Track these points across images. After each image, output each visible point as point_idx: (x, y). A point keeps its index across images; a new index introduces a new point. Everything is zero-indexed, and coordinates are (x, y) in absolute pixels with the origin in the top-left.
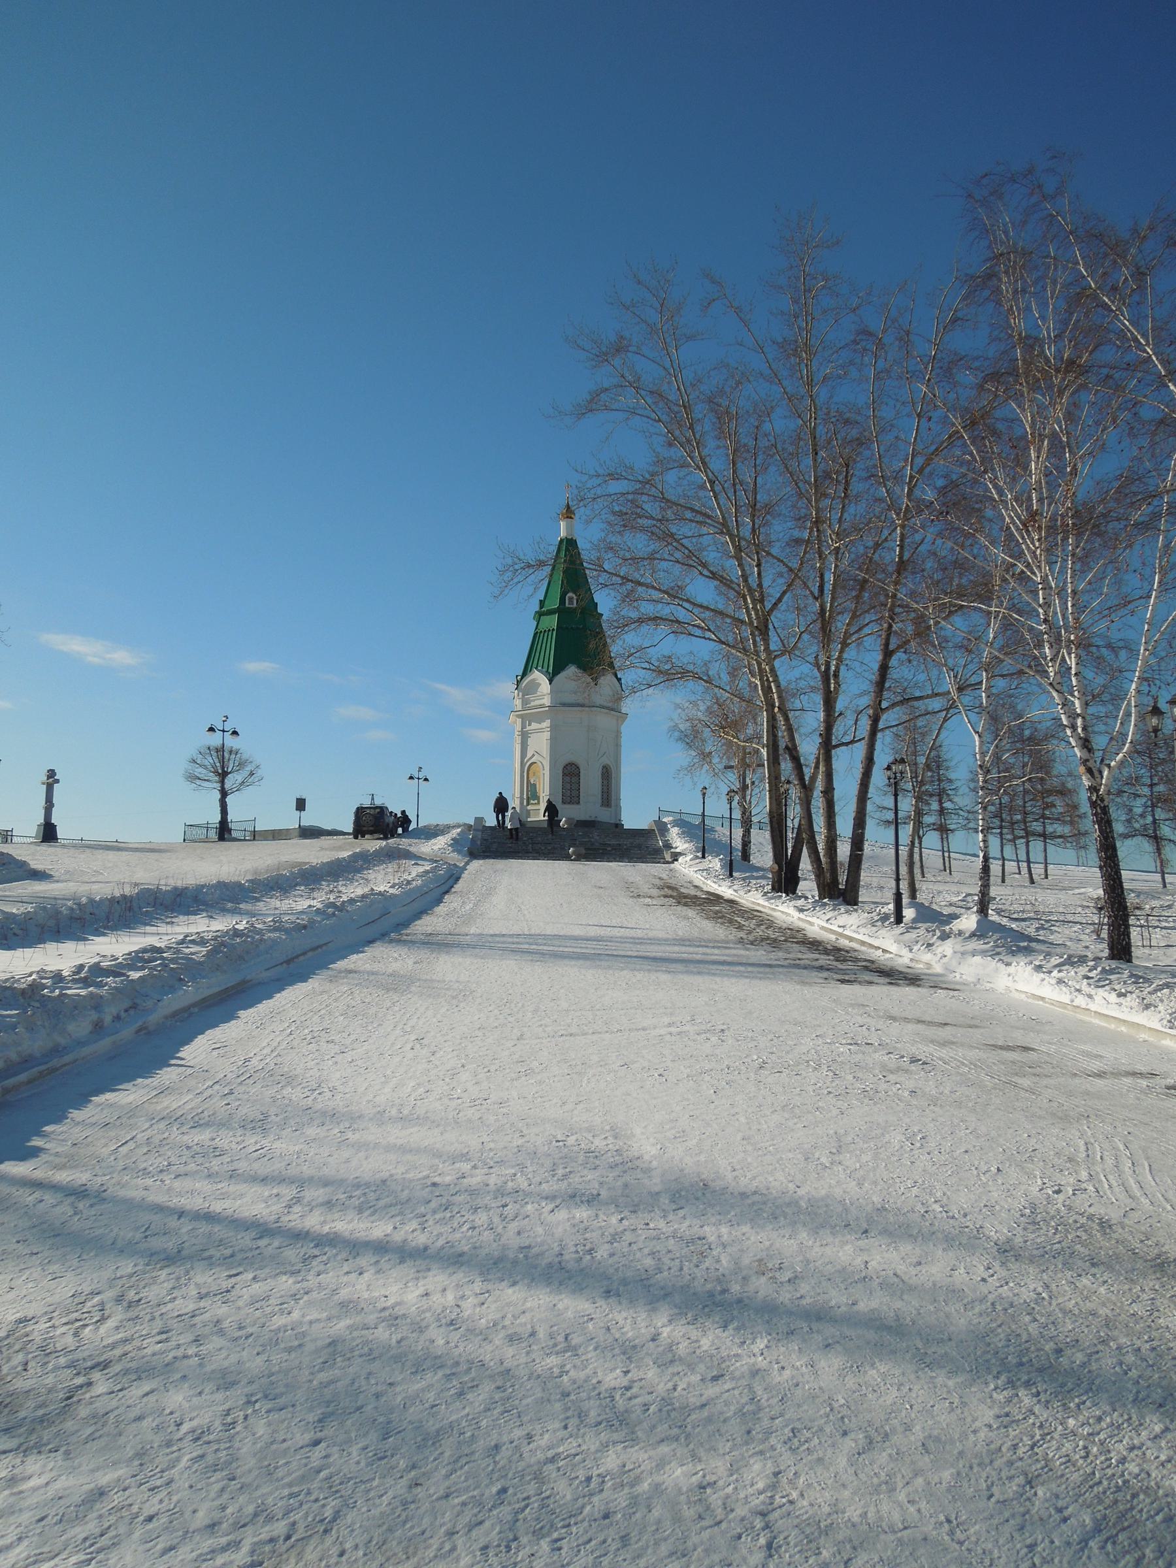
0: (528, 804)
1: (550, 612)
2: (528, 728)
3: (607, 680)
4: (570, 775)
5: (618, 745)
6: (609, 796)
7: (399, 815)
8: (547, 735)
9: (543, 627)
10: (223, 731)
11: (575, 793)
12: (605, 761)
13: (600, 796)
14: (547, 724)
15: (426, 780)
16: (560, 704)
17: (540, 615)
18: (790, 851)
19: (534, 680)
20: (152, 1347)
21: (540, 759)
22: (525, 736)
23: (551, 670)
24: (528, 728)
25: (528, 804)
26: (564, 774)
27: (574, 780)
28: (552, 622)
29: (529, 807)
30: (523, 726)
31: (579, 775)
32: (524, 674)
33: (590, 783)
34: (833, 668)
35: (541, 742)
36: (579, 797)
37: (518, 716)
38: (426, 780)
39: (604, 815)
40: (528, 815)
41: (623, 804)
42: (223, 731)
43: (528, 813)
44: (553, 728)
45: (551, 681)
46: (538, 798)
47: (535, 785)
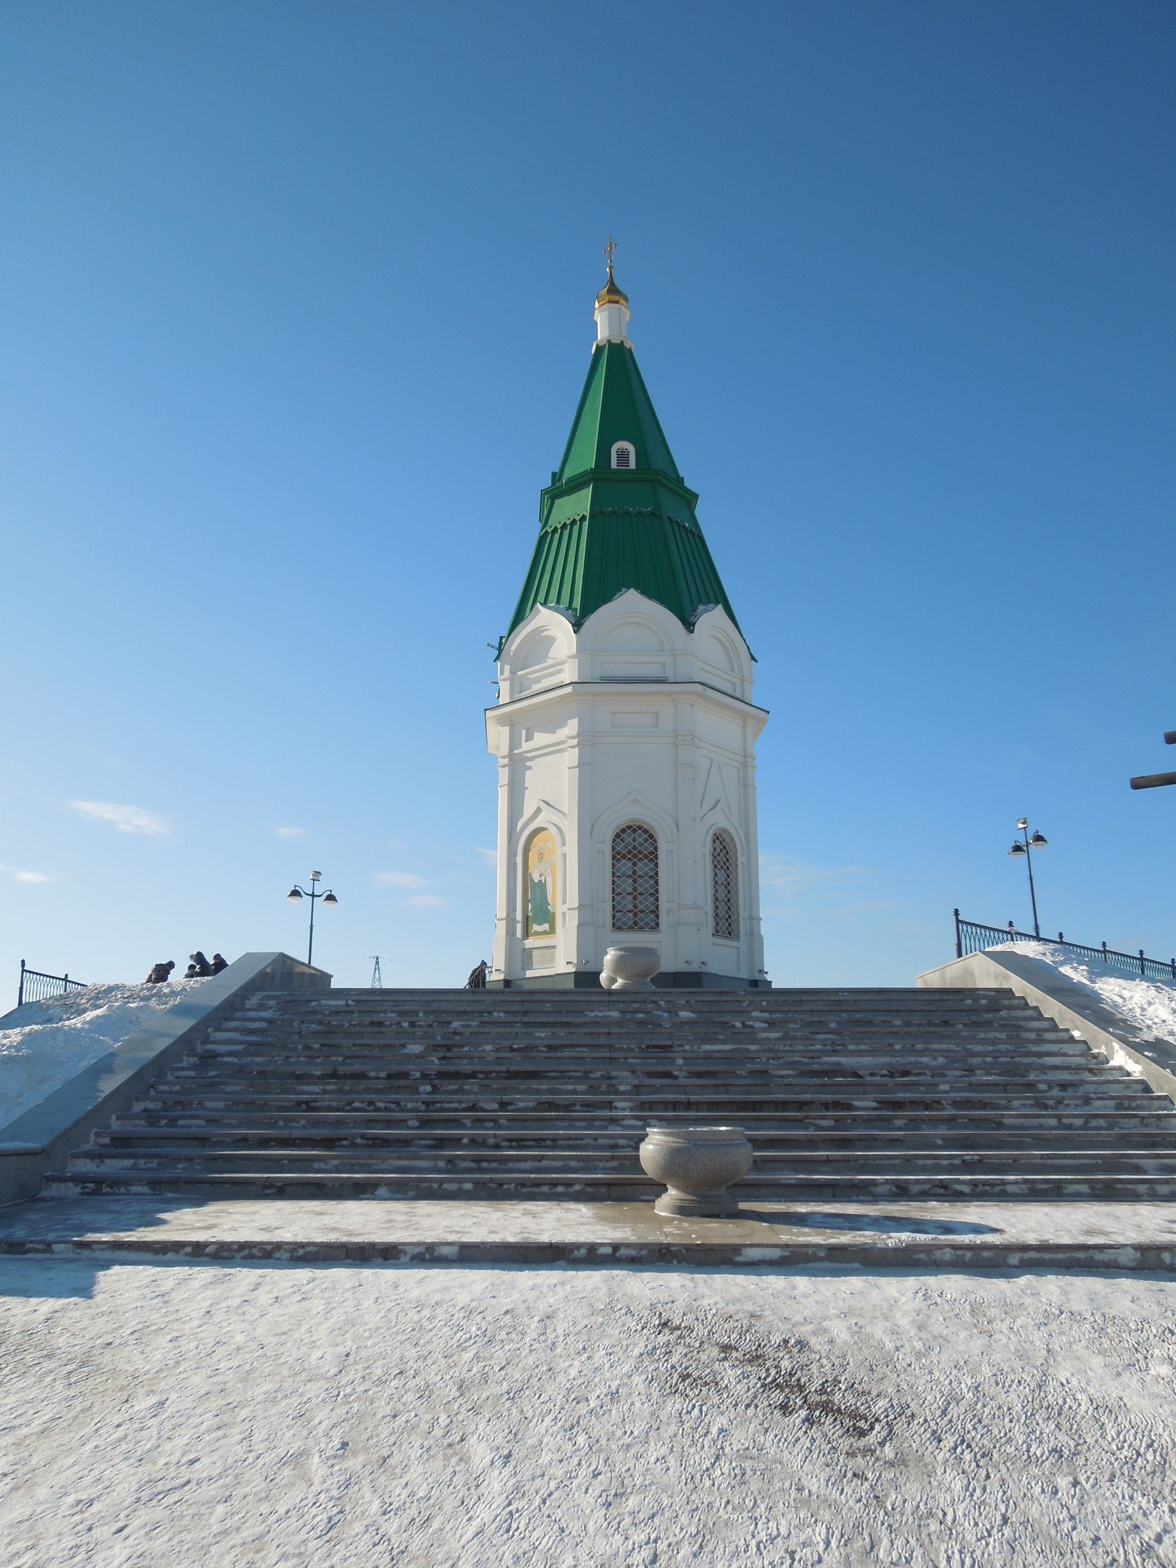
0: (526, 934)
1: (576, 485)
2: (526, 746)
3: (711, 619)
4: (631, 861)
5: (746, 787)
6: (730, 914)
7: (211, 961)
8: (571, 756)
9: (556, 520)
10: (313, 895)
11: (645, 903)
12: (717, 820)
13: (709, 909)
14: (572, 727)
15: (331, 898)
16: (601, 681)
17: (558, 490)
18: (35, 1027)
19: (538, 631)
20: (343, 1478)
21: (555, 818)
22: (517, 765)
23: (577, 603)
24: (526, 746)
25: (526, 934)
26: (617, 856)
27: (642, 867)
28: (580, 504)
29: (530, 943)
30: (514, 743)
31: (653, 857)
32: (519, 618)
33: (684, 878)
34: (214, 1435)
35: (555, 779)
36: (655, 912)
37: (501, 720)
38: (331, 898)
39: (721, 959)
40: (527, 963)
41: (766, 929)
42: (313, 895)
43: (527, 959)
44: (588, 741)
45: (577, 626)
46: (549, 918)
47: (542, 886)
